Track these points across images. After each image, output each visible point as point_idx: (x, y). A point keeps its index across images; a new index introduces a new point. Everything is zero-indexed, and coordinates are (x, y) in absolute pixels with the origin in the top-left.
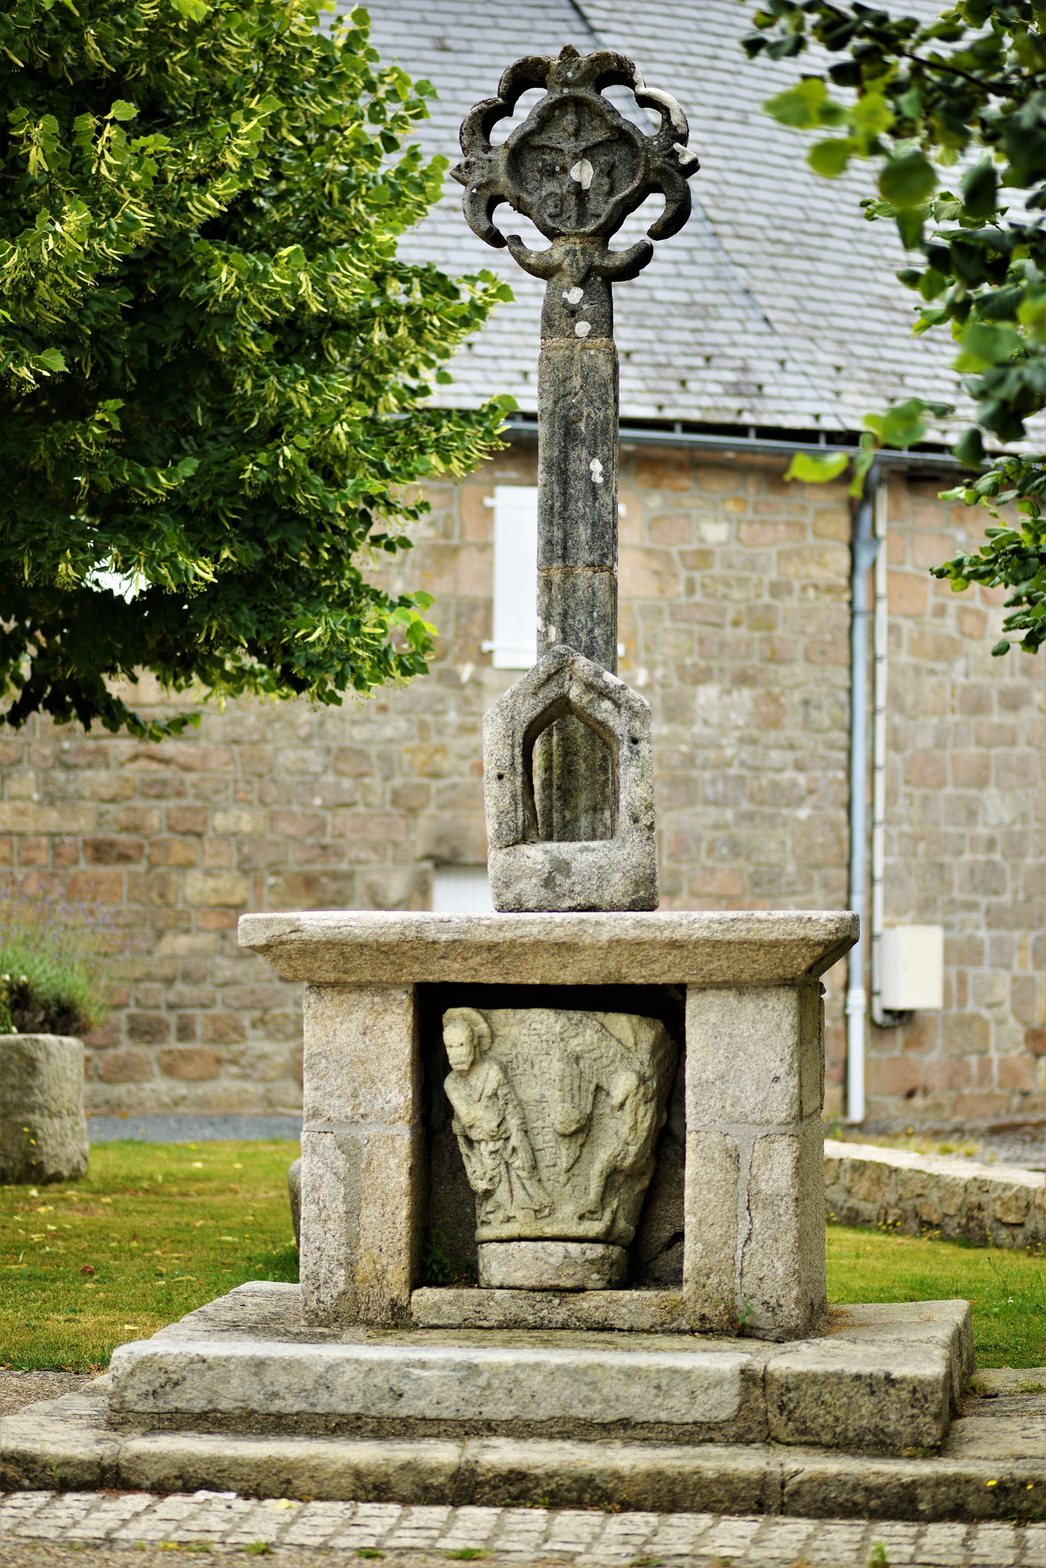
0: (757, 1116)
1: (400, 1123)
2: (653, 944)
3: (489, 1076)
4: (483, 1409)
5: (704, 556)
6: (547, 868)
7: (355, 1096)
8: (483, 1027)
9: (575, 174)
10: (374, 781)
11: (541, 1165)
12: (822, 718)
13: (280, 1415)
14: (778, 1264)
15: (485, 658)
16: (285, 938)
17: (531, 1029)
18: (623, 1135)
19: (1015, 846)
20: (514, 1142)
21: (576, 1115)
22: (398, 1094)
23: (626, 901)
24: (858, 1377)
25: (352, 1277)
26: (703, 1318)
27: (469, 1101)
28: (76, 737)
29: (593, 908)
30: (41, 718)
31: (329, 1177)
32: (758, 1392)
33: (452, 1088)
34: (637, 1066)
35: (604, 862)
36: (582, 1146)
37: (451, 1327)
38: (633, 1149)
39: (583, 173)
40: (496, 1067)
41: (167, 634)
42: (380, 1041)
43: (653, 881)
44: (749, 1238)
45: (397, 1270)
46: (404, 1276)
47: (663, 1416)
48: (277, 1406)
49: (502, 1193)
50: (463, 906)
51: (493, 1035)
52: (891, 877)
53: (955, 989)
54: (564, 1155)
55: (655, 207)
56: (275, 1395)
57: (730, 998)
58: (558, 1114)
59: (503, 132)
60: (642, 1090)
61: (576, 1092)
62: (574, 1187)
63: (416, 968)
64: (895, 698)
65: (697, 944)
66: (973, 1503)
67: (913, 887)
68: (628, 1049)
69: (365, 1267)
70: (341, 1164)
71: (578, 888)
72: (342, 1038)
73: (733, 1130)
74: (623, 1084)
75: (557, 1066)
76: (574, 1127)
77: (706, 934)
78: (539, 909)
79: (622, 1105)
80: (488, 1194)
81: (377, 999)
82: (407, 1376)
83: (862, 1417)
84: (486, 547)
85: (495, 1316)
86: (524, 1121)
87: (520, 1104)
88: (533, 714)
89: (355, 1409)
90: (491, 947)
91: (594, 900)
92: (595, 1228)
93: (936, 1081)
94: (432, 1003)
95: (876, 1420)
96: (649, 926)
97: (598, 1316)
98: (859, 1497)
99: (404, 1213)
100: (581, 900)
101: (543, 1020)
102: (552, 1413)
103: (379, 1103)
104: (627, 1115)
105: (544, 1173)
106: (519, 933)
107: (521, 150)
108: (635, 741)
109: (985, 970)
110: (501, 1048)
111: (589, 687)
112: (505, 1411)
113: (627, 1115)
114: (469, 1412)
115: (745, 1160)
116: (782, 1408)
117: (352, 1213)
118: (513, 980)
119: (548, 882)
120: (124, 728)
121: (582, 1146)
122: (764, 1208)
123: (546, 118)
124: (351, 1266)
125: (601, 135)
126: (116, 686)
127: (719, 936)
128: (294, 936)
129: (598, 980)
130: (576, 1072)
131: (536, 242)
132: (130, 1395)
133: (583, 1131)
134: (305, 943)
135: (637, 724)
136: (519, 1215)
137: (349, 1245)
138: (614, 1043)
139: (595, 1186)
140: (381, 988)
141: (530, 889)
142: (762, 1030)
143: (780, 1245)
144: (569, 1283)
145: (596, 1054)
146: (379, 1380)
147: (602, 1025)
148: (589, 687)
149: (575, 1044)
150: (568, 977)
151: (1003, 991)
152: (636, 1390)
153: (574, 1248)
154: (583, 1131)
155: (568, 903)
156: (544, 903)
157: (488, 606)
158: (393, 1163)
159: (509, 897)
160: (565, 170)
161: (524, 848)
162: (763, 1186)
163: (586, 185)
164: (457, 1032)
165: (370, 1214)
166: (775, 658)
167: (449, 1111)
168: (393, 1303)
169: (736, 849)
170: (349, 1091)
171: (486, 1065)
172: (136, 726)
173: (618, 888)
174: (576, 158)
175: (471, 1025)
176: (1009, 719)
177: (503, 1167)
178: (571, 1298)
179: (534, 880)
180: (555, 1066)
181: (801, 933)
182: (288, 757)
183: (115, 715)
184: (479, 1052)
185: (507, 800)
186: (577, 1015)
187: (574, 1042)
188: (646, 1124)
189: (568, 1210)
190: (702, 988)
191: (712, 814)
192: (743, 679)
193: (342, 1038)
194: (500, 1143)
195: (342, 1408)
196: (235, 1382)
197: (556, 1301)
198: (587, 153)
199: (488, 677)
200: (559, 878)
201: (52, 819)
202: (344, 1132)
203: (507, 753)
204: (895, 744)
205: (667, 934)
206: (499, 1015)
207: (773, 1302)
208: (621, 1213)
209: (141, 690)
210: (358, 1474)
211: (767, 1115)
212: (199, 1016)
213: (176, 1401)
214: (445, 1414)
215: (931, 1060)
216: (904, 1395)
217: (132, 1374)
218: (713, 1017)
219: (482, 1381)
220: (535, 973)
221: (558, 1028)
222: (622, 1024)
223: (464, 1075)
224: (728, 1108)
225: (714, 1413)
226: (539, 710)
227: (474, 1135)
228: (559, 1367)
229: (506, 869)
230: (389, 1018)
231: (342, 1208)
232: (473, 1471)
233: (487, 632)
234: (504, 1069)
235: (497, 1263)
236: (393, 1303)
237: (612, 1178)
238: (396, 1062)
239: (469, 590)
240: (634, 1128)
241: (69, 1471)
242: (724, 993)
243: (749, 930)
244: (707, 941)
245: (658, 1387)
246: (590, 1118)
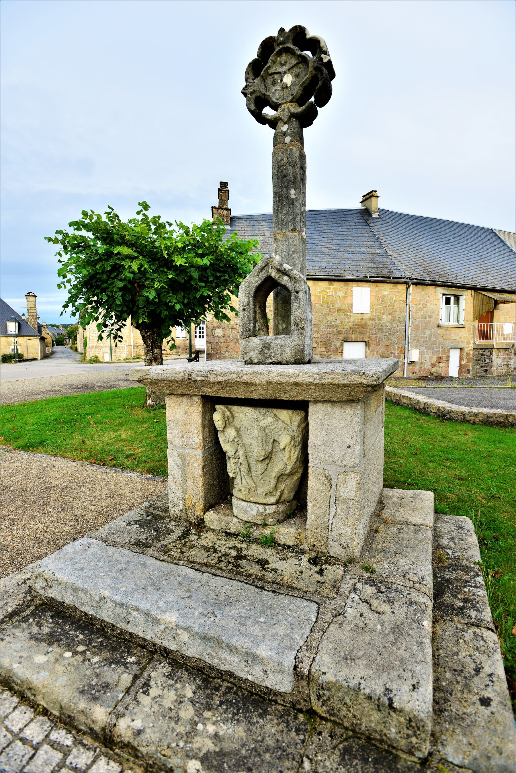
0: (340, 463)
1: (198, 449)
2: (286, 384)
3: (231, 433)
4: (162, 641)
5: (384, 296)
6: (261, 346)
8: (228, 413)
10: (335, 330)
11: (252, 470)
12: (402, 320)
14: (348, 529)
15: (351, 312)
16: (144, 377)
17: (245, 415)
18: (286, 460)
19: (430, 338)
21: (263, 453)
23: (292, 360)
29: (279, 363)
32: (305, 683)
34: (291, 432)
35: (283, 344)
36: (268, 464)
40: (234, 430)
42: (190, 417)
43: (303, 352)
44: (335, 515)
45: (199, 506)
46: (202, 507)
51: (233, 416)
52: (411, 343)
53: (421, 358)
57: (328, 408)
58: (257, 452)
60: (293, 442)
61: (264, 443)
62: (264, 481)
64: (412, 316)
65: (307, 385)
67: (415, 344)
68: (287, 425)
69: (189, 502)
70: (179, 462)
71: (273, 355)
72: (178, 415)
73: (329, 468)
74: (284, 440)
76: (262, 458)
77: (310, 380)
78: (259, 363)
79: (284, 449)
81: (189, 400)
83: (371, 721)
84: (352, 296)
86: (245, 452)
87: (244, 445)
88: (257, 284)
91: (280, 359)
92: (273, 500)
93: (417, 371)
96: (284, 375)
99: (201, 484)
100: (274, 359)
102: (194, 655)
105: (253, 473)
106: (228, 377)
108: (297, 292)
109: (425, 355)
110: (236, 422)
111: (279, 271)
113: (286, 453)
115: (334, 482)
118: (234, 396)
119: (262, 352)
121: (268, 464)
122: (342, 503)
127: (317, 381)
128: (147, 377)
129: (267, 398)
130: (264, 434)
133: (268, 457)
134: (152, 380)
135: (297, 285)
137: (183, 492)
138: (281, 422)
140: (190, 396)
141: (254, 355)
142: (343, 423)
143: (349, 521)
145: (272, 427)
147: (275, 415)
148: (279, 271)
149: (263, 423)
150: (255, 396)
151: (428, 359)
153: (261, 508)
154: (268, 457)
155: (270, 361)
156: (261, 361)
157: (352, 305)
159: (247, 359)
161: (253, 338)
162: (342, 494)
165: (190, 482)
166: (395, 311)
169: (388, 338)
170: (181, 435)
171: (230, 429)
173: (288, 354)
177: (238, 469)
179: (256, 352)
181: (359, 380)
182: (322, 327)
184: (227, 422)
185: (246, 319)
187: (263, 422)
188: (295, 457)
190: (316, 402)
191: (385, 334)
192: (390, 314)
193: (178, 415)
194: (236, 460)
197: (255, 528)
199: (352, 314)
200: (266, 351)
202: (180, 451)
203: (246, 300)
204: (412, 323)
205: (292, 379)
207: (345, 545)
208: (286, 490)
211: (344, 462)
215: (417, 368)
222: (284, 414)
223: (223, 431)
224: (327, 458)
225: (278, 687)
226: (259, 282)
229: (245, 347)
230: (193, 408)
231: (181, 479)
233: (352, 308)
234: (238, 431)
238: (196, 425)
239: (349, 302)
240: (290, 458)
242: (325, 405)
243: (332, 379)
244: (311, 384)
246: (271, 453)
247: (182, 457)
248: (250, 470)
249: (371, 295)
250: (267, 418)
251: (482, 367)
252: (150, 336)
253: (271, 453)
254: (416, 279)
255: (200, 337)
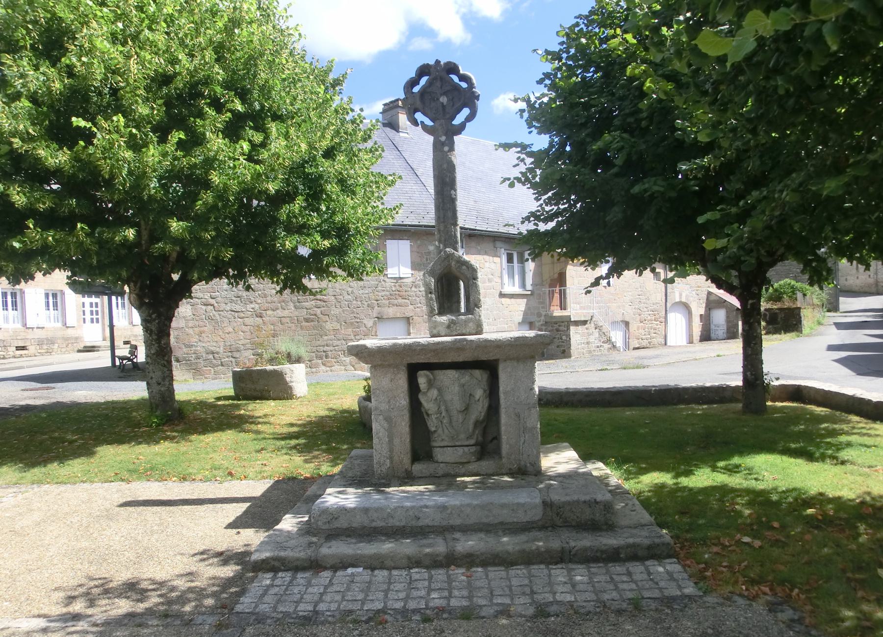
5: (429, 253)
7: (389, 402)
9: (441, 99)
13: (375, 528)
17: (448, 377)
18: (479, 409)
20: (443, 414)
22: (404, 401)
24: (585, 502)
25: (391, 462)
26: (510, 469)
27: (428, 402)
28: (298, 296)
30: (288, 291)
31: (382, 430)
32: (549, 509)
33: (422, 399)
37: (426, 477)
38: (483, 414)
39: (444, 100)
41: (317, 264)
45: (406, 459)
47: (515, 520)
48: (374, 524)
49: (440, 431)
50: (421, 336)
51: (435, 379)
54: (461, 417)
55: (466, 112)
56: (373, 521)
58: (457, 404)
59: (416, 89)
63: (409, 359)
66: (640, 553)
69: (396, 458)
70: (386, 425)
74: (479, 393)
75: (457, 388)
80: (435, 431)
82: (421, 511)
85: (441, 473)
86: (446, 407)
89: (402, 524)
90: (434, 351)
92: (472, 442)
94: (413, 370)
95: (592, 516)
97: (475, 471)
98: (598, 554)
101: (452, 374)
103: (398, 404)
104: (481, 403)
105: (454, 424)
107: (423, 92)
112: (458, 522)
113: (481, 403)
114: (444, 523)
116: (558, 514)
117: (391, 442)
120: (308, 293)
123: (429, 84)
124: (391, 458)
125: (448, 88)
126: (305, 281)
129: (470, 360)
131: (429, 122)
132: (320, 523)
136: (446, 438)
139: (471, 427)
144: (465, 461)
146: (411, 513)
149: (463, 381)
150: (460, 359)
152: (505, 511)
153: (466, 449)
154: (466, 410)
158: (403, 424)
159: (435, 332)
160: (438, 99)
163: (445, 103)
164: (422, 380)
165: (397, 441)
167: (420, 404)
168: (406, 470)
172: (312, 293)
174: (441, 95)
175: (427, 376)
176: (490, 284)
178: (466, 465)
180: (456, 389)
183: (305, 289)
184: (431, 384)
186: (463, 371)
189: (462, 436)
195: (398, 524)
196: (358, 517)
198: (445, 94)
201: (297, 313)
206: (437, 372)
209: (311, 282)
210: (409, 558)
212: (330, 353)
213: (336, 524)
214: (436, 524)
216: (602, 507)
217: (320, 516)
218: (509, 370)
219: (449, 512)
220: (449, 359)
221: (457, 376)
222: (477, 373)
223: (425, 393)
227: (430, 412)
228: (477, 505)
230: (399, 376)
232: (453, 554)
234: (439, 390)
235: (440, 455)
236: (406, 470)
237: (477, 423)
241: (299, 563)
245: (513, 510)
246: (468, 405)
247: (388, 419)
248: (451, 422)
249: (412, 251)
250: (466, 377)
251: (558, 347)
252: (155, 320)
253: (468, 405)
254: (471, 229)
255: (92, 320)
